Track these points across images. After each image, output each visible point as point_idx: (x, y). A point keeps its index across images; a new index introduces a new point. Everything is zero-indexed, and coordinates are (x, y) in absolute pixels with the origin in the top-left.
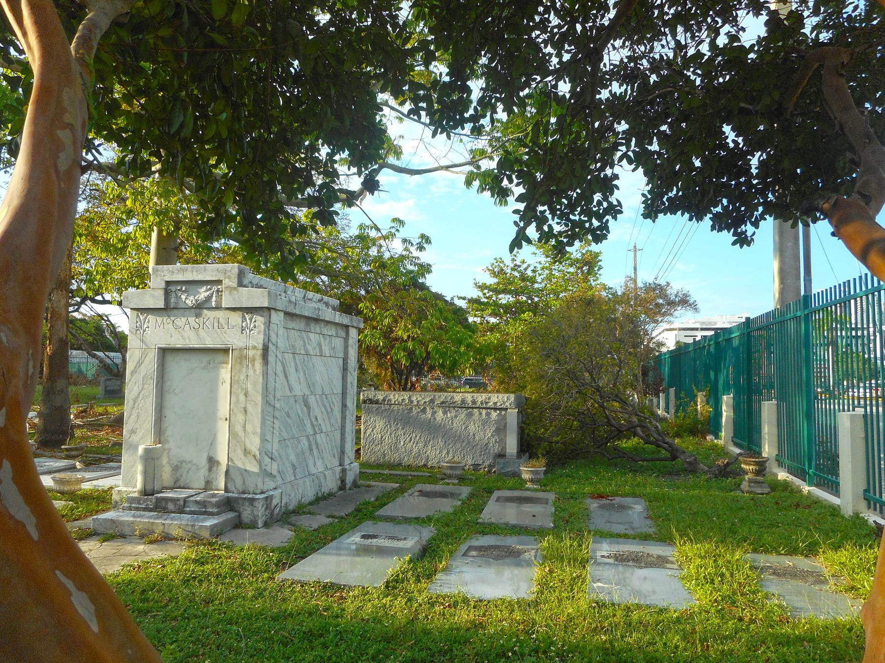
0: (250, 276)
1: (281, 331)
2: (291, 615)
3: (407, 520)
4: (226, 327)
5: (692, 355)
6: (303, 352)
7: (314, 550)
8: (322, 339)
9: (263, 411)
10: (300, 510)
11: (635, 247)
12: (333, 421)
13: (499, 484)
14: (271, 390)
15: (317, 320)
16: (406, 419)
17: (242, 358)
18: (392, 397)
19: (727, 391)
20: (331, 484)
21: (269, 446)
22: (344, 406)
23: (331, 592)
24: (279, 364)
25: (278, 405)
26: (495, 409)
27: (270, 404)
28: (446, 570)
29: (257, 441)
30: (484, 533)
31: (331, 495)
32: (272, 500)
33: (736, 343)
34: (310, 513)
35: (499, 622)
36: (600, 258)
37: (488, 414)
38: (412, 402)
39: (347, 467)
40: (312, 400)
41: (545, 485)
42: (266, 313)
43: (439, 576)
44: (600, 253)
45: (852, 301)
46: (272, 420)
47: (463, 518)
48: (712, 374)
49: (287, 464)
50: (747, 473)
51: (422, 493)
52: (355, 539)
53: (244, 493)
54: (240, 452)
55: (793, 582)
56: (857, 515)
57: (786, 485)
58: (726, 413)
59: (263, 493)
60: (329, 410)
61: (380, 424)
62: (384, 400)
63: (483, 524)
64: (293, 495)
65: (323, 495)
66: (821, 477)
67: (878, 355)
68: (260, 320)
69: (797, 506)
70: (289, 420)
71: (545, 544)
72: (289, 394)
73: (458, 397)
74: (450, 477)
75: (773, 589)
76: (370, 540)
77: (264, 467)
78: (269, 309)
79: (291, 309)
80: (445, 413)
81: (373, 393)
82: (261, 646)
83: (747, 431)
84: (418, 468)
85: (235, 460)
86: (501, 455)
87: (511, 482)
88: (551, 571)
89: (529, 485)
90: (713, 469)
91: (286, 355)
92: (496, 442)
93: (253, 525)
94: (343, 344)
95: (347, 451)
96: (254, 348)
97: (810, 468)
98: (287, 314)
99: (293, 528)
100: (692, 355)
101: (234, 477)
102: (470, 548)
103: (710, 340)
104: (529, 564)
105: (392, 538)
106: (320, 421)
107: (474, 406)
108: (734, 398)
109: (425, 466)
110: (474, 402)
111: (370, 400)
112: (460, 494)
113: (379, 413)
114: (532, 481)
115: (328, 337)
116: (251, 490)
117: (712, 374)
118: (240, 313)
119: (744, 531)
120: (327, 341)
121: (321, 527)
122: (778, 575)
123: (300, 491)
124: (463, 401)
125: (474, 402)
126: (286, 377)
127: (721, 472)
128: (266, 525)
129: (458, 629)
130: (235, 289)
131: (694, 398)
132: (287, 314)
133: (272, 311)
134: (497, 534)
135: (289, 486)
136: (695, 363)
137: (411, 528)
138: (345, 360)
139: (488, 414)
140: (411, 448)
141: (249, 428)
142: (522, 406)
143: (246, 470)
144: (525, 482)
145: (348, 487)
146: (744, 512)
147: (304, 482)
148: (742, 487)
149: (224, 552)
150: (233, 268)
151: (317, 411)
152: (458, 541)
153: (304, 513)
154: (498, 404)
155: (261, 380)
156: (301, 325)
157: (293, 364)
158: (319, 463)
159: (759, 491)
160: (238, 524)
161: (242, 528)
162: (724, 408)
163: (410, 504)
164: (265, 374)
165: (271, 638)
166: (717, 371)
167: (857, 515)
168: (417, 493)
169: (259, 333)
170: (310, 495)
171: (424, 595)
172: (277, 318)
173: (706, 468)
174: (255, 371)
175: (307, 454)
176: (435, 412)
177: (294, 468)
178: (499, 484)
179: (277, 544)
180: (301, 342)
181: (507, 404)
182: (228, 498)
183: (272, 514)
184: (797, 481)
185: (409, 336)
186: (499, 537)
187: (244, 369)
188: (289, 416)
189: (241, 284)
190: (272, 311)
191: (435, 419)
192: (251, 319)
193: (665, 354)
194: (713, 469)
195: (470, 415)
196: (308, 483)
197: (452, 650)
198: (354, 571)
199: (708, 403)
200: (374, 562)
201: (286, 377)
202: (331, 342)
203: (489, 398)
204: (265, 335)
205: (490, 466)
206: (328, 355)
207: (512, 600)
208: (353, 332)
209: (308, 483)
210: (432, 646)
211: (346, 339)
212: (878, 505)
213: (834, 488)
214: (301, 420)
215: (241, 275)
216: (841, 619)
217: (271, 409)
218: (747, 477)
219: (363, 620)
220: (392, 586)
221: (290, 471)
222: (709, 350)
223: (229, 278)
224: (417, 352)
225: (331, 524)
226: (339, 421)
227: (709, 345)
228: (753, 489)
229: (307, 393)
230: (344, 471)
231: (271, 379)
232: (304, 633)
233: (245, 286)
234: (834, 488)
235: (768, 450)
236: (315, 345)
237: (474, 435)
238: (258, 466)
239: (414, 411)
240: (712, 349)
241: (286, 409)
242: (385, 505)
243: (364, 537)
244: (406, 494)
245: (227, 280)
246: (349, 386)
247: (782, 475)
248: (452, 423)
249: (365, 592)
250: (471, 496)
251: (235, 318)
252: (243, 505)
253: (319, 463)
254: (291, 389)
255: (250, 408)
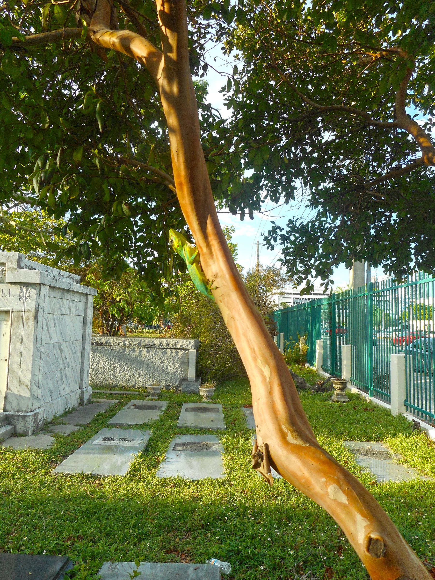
0: (25, 261)
1: (47, 299)
2: (70, 499)
3: (131, 427)
4: (8, 296)
5: (296, 313)
6: (59, 313)
7: (73, 451)
8: (71, 304)
9: (33, 354)
10: (54, 422)
11: (258, 242)
12: (76, 359)
13: (185, 399)
14: (39, 339)
15: (68, 291)
16: (121, 356)
17: (19, 317)
18: (112, 341)
19: (319, 335)
20: (74, 402)
21: (36, 378)
22: (83, 348)
23: (92, 481)
24: (45, 321)
25: (43, 350)
26: (181, 349)
27: (38, 350)
28: (164, 461)
29: (29, 375)
30: (183, 434)
31: (73, 410)
32: (38, 416)
33: (325, 308)
34: (62, 423)
35: (209, 496)
36: (236, 248)
37: (176, 353)
38: (126, 344)
39: (85, 390)
40: (63, 345)
41: (214, 399)
42: (38, 287)
43: (160, 465)
44: (237, 245)
45: (400, 289)
46: (39, 360)
47: (167, 424)
48: (309, 327)
49: (47, 390)
50: (336, 390)
51: (137, 407)
52: (98, 440)
53: (18, 411)
54: (16, 383)
55: (373, 459)
56: (400, 415)
57: (357, 397)
58: (319, 351)
59: (32, 411)
60: (74, 351)
61: (103, 359)
62: (106, 343)
63: (180, 427)
64: (50, 412)
65: (69, 410)
66: (378, 391)
67: (394, 312)
68: (33, 292)
69: (366, 409)
70: (49, 360)
71: (224, 440)
72: (49, 342)
73: (157, 342)
74: (153, 395)
75: (363, 464)
76: (109, 442)
77: (33, 393)
78: (40, 284)
79: (53, 284)
80: (148, 352)
81: (99, 338)
82: (56, 523)
83: (332, 362)
84: (128, 389)
85: (12, 388)
86: (185, 380)
87: (193, 398)
88: (232, 459)
89: (204, 399)
90: (315, 387)
91: (48, 315)
92: (181, 371)
93: (25, 434)
94: (84, 307)
95: (84, 379)
96: (29, 311)
97: (371, 386)
98: (51, 287)
99: (54, 435)
100: (296, 313)
101: (11, 400)
102: (176, 445)
103: (308, 305)
104: (214, 454)
105: (124, 440)
106: (68, 359)
107: (168, 347)
108: (323, 342)
109: (133, 387)
110: (167, 345)
111: (96, 343)
112: (161, 407)
113: (102, 351)
114: (207, 397)
115: (74, 302)
116: (24, 410)
117: (309, 327)
118: (18, 286)
119: (340, 427)
120: (74, 304)
121: (73, 433)
122: (364, 454)
123: (55, 408)
124: (160, 344)
125: (167, 345)
126: (48, 330)
127: (319, 389)
128: (34, 433)
129: (185, 502)
130: (15, 269)
131: (297, 340)
132: (51, 287)
133: (42, 285)
134: (192, 434)
135: (48, 405)
136: (298, 318)
137: (140, 432)
138: (85, 317)
139: (176, 353)
140: (124, 375)
141: (23, 366)
142: (199, 346)
143: (20, 396)
144: (202, 397)
145: (85, 403)
146: (337, 414)
147: (58, 401)
148: (333, 398)
149: (8, 455)
150: (14, 255)
151: (67, 353)
152: (167, 440)
153: (59, 424)
154: (184, 346)
155: (33, 333)
156: (58, 294)
157: (52, 321)
158: (67, 388)
159: (343, 400)
160: (14, 434)
161: (17, 436)
162: (317, 347)
163: (128, 415)
164: (36, 329)
165: (61, 517)
166: (313, 325)
167: (400, 415)
168: (132, 407)
169: (32, 300)
170: (61, 411)
171: (156, 479)
172: (45, 290)
173: (310, 386)
174: (28, 327)
175: (60, 382)
176: (142, 351)
177: (51, 392)
178: (185, 399)
179: (44, 447)
180: (58, 306)
181: (189, 346)
182: (7, 415)
183: (38, 425)
184: (364, 394)
185: (120, 299)
186: (192, 436)
187: (21, 326)
188: (49, 357)
189: (19, 266)
190: (42, 285)
191: (141, 356)
192: (26, 291)
193: (277, 311)
194: (315, 387)
195: (165, 353)
196: (60, 402)
197: (183, 517)
198: (106, 463)
199: (306, 343)
200: (118, 459)
201: (48, 330)
202: (76, 306)
203: (178, 342)
204: (36, 302)
205: (177, 386)
206: (74, 314)
207: (213, 480)
208: (91, 299)
209: (60, 402)
210: (170, 514)
211: (86, 303)
212: (412, 409)
213: (387, 399)
214: (57, 360)
215: (20, 259)
216: (408, 481)
217: (39, 353)
218: (335, 392)
219: (120, 499)
220: (134, 472)
221: (49, 394)
222: (307, 311)
223: (11, 261)
224: (126, 309)
225: (79, 430)
226: (80, 359)
227: (308, 308)
228: (339, 399)
229: (61, 340)
230: (82, 393)
231: (39, 332)
232: (83, 511)
233: (22, 268)
234: (387, 399)
235: (345, 375)
236: (66, 307)
237: (167, 366)
238: (29, 393)
239: (127, 350)
240: (310, 310)
241: (47, 353)
242: (113, 415)
243: (105, 439)
244: (126, 407)
245: (9, 263)
246: (87, 335)
247: (354, 390)
248: (153, 358)
249: (116, 479)
250: (169, 408)
251: (15, 290)
252: (18, 420)
253: (67, 388)
254: (51, 338)
255: (24, 353)
